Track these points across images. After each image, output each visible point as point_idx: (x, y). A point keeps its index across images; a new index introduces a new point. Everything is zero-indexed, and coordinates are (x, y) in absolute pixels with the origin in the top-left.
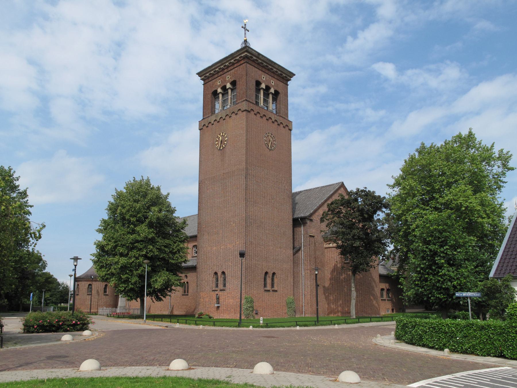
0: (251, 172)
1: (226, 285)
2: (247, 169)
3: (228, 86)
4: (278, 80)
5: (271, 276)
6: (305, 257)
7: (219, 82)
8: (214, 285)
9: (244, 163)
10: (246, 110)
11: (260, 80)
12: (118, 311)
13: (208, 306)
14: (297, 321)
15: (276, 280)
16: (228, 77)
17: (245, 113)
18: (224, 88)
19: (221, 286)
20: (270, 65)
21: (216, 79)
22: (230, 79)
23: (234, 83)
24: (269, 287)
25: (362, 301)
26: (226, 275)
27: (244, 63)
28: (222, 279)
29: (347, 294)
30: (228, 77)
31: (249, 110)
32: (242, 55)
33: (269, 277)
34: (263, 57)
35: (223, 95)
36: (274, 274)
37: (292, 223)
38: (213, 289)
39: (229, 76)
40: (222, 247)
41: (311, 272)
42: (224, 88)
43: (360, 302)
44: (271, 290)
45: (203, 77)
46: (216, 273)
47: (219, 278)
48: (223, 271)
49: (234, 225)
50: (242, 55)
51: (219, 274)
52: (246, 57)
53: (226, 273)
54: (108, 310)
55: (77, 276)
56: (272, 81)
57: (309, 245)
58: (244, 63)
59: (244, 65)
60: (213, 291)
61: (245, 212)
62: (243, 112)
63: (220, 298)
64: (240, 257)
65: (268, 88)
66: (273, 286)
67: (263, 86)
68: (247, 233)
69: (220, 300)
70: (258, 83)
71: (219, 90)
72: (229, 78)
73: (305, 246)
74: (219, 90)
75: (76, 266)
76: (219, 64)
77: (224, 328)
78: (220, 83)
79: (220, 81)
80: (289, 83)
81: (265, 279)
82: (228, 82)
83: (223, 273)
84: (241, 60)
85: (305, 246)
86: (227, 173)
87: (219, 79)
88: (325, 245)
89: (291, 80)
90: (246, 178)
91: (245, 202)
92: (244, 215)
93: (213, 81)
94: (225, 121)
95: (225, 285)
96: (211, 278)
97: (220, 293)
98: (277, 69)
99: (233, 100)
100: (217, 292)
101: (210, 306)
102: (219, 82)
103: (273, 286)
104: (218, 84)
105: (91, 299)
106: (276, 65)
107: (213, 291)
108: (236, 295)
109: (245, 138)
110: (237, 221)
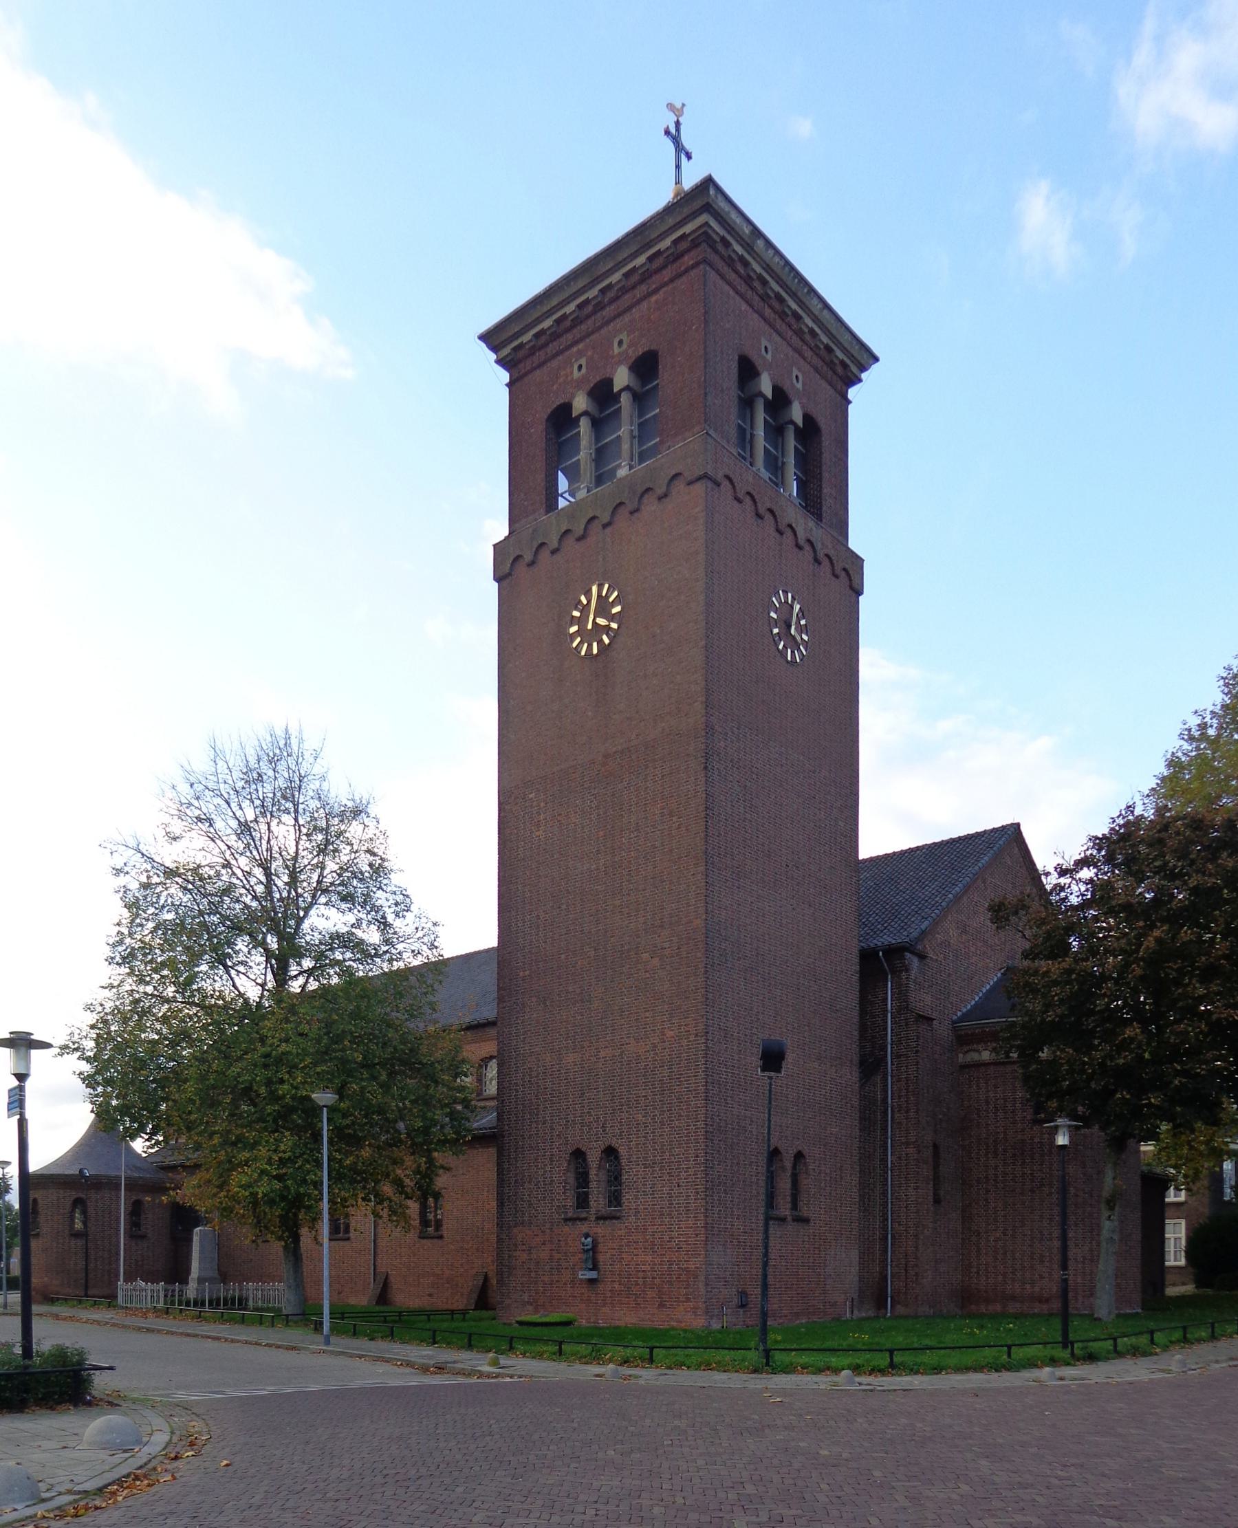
0: (722, 743)
1: (624, 1200)
2: (709, 727)
3: (622, 377)
4: (816, 370)
5: (788, 1164)
6: (900, 1097)
7: (580, 367)
8: (571, 1201)
9: (699, 706)
10: (705, 476)
11: (754, 358)
12: (191, 1290)
13: (546, 1279)
14: (1010, 1342)
15: (806, 1182)
16: (620, 342)
17: (699, 488)
18: (603, 394)
19: (598, 1201)
20: (794, 295)
21: (567, 353)
22: (629, 347)
23: (646, 367)
24: (784, 1209)
25: (1092, 1260)
26: (624, 1162)
27: (693, 267)
28: (603, 1176)
29: (1041, 1232)
30: (620, 342)
31: (719, 477)
32: (688, 228)
33: (783, 1169)
34: (771, 252)
35: (598, 425)
36: (799, 1156)
37: (857, 968)
38: (570, 1215)
39: (624, 336)
40: (602, 1054)
41: (919, 1152)
42: (603, 394)
43: (1083, 1263)
44: (789, 1218)
45: (506, 351)
46: (579, 1155)
47: (593, 1172)
48: (607, 1144)
49: (656, 961)
50: (688, 228)
51: (594, 1157)
52: (703, 236)
53: (622, 1151)
54: (151, 1291)
55: (34, 1166)
56: (795, 372)
57: (917, 1052)
58: (693, 267)
59: (693, 273)
60: (566, 1220)
61: (702, 910)
62: (691, 487)
63: (601, 1247)
64: (763, 1071)
65: (779, 402)
66: (795, 1206)
67: (766, 386)
68: (710, 996)
69: (601, 1258)
70: (747, 370)
71: (580, 403)
72: (625, 346)
73: (899, 1056)
74: (580, 403)
75: (21, 1077)
76: (581, 283)
77: (719, 1378)
78: (584, 370)
79: (583, 361)
80: (852, 393)
81: (771, 1178)
82: (620, 363)
83: (610, 1152)
84: (680, 256)
85: (899, 1056)
86: (622, 752)
87: (580, 354)
88: (961, 1055)
89: (860, 380)
90: (706, 768)
91: (702, 869)
92: (699, 922)
93: (554, 364)
94: (608, 530)
95: (615, 1198)
96: (559, 1175)
97: (601, 1230)
98: (816, 320)
99: (640, 445)
100: (584, 1228)
101: (555, 1278)
102: (580, 367)
103: (795, 1206)
104: (576, 374)
105: (87, 1253)
106: (815, 301)
107: (566, 1220)
108: (666, 1238)
109: (702, 597)
110: (666, 945)
